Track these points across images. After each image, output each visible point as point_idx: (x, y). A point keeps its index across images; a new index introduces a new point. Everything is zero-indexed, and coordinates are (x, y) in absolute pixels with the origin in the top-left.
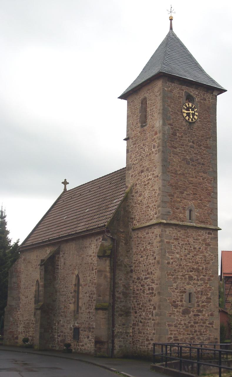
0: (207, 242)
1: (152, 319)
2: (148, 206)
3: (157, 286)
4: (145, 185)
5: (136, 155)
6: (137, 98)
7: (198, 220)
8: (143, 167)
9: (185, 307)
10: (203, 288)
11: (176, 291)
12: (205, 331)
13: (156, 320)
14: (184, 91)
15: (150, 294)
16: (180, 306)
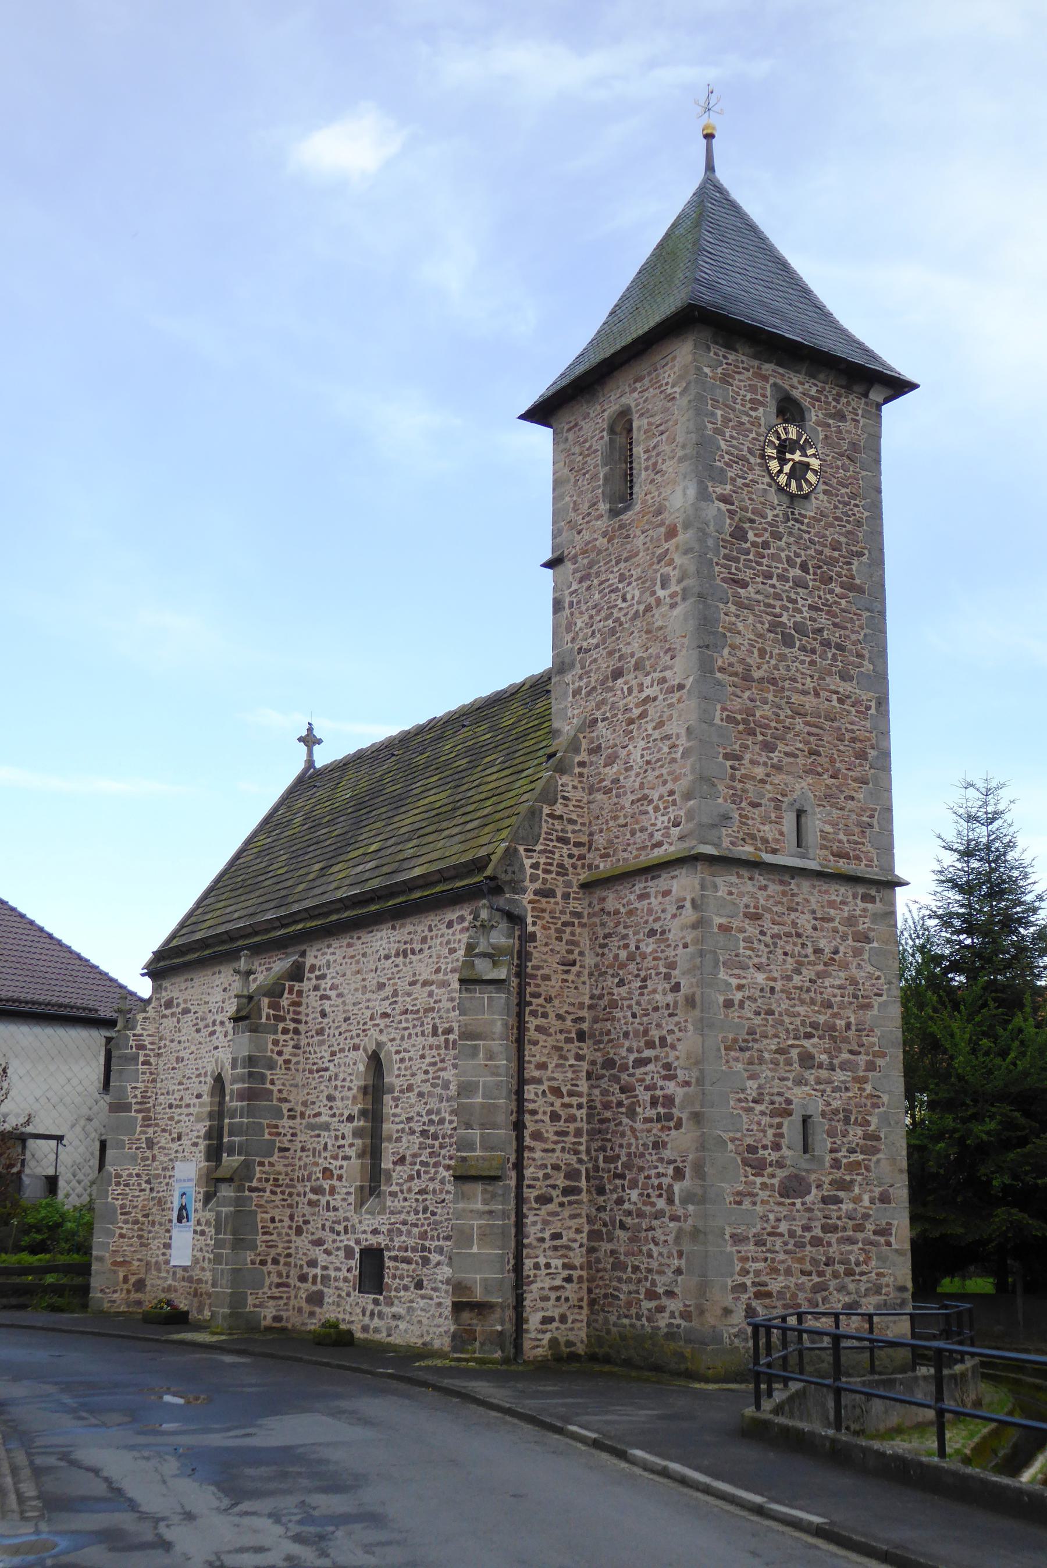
0: (861, 927)
1: (668, 1215)
2: (645, 797)
3: (686, 1089)
4: (631, 722)
5: (591, 617)
6: (592, 415)
7: (826, 848)
8: (621, 658)
9: (792, 1169)
10: (850, 1098)
11: (759, 1108)
12: (861, 1259)
13: (686, 1221)
14: (771, 381)
15: (659, 1120)
16: (771, 1165)
